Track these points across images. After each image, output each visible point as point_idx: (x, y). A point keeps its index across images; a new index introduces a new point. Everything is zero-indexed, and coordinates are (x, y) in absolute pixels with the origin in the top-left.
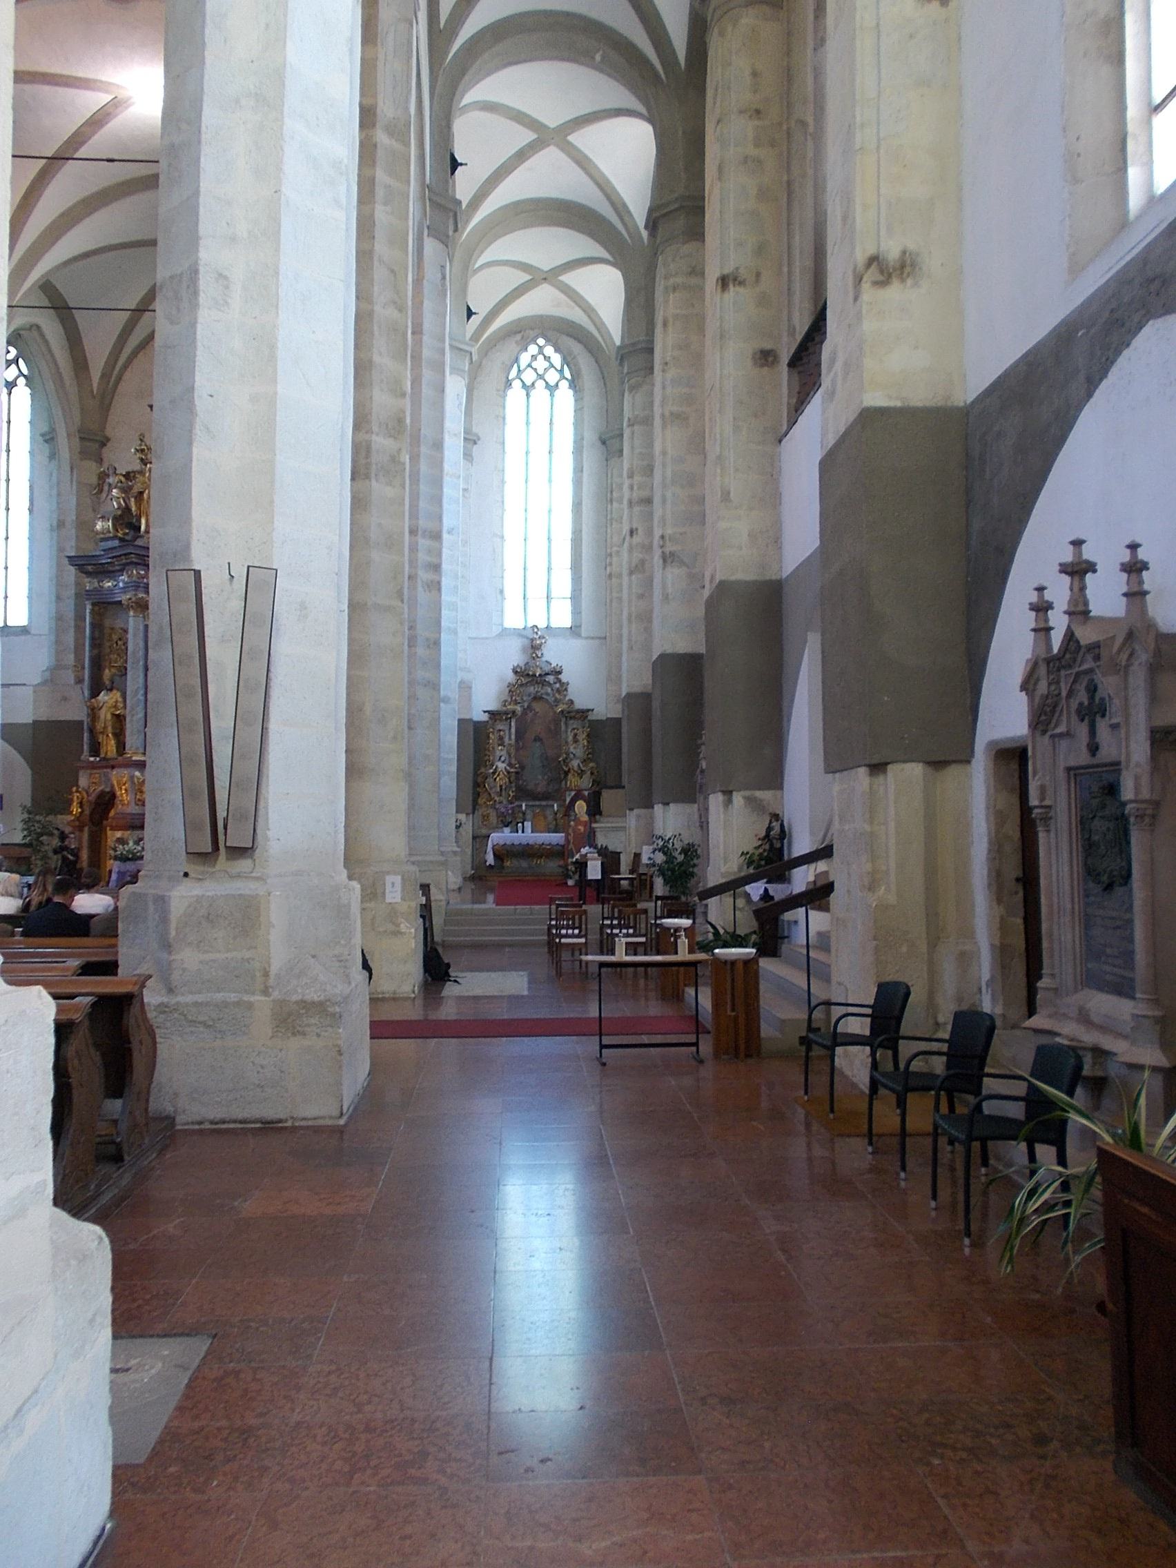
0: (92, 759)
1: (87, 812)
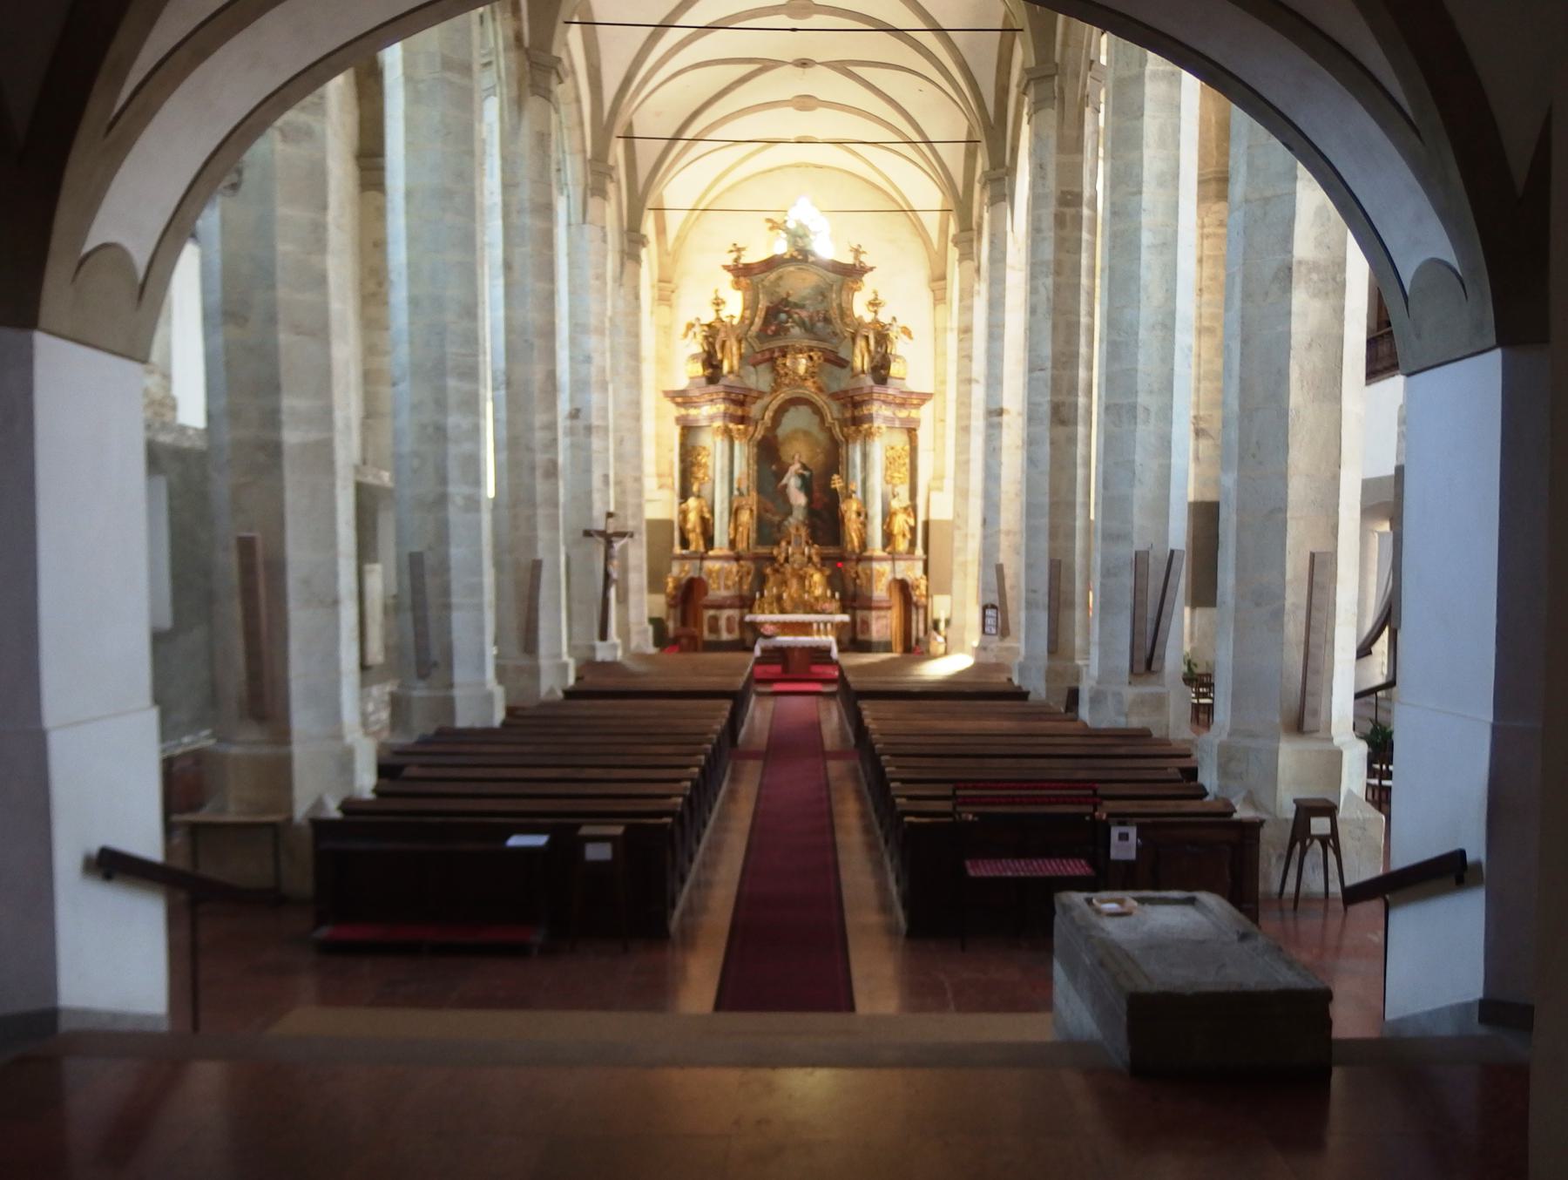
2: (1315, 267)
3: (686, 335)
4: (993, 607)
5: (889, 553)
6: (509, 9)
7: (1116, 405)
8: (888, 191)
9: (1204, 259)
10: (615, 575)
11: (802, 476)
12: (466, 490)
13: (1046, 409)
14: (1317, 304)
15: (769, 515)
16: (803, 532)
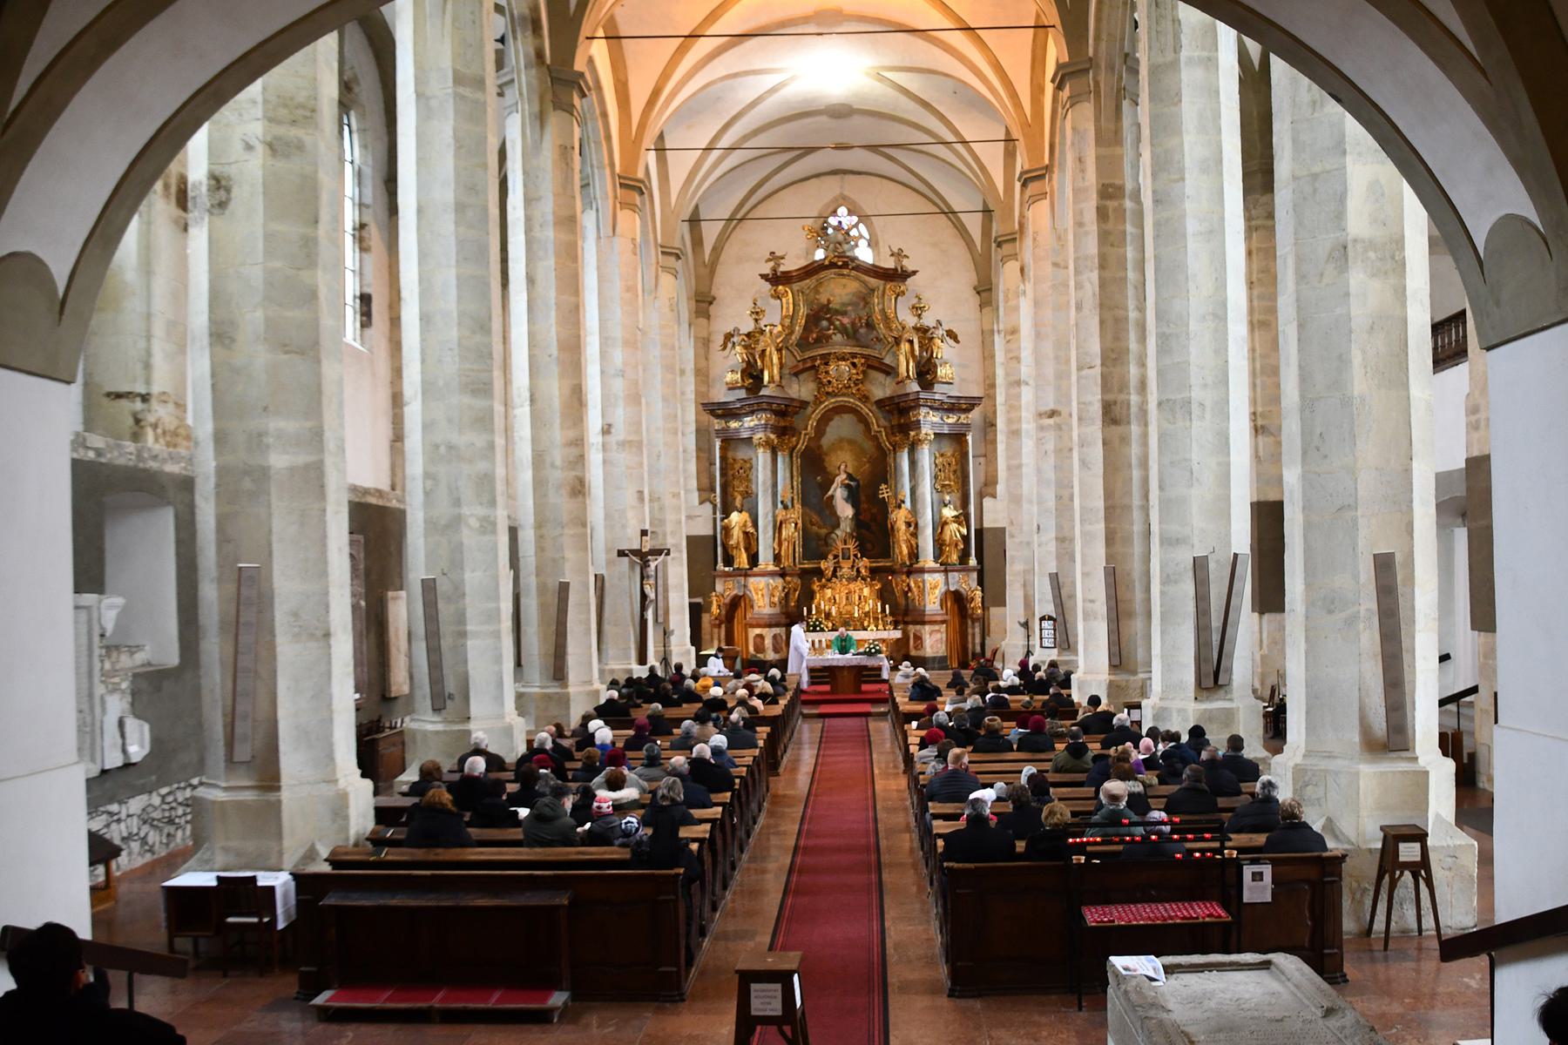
0: (727, 569)
1: (724, 612)
2: (1371, 245)
3: (724, 347)
4: (1050, 618)
6: (530, 27)
7: (1168, 400)
9: (1254, 252)
10: (652, 596)
11: (847, 487)
12: (481, 511)
13: (1096, 409)
14: (1376, 284)
15: (815, 528)
16: (851, 546)
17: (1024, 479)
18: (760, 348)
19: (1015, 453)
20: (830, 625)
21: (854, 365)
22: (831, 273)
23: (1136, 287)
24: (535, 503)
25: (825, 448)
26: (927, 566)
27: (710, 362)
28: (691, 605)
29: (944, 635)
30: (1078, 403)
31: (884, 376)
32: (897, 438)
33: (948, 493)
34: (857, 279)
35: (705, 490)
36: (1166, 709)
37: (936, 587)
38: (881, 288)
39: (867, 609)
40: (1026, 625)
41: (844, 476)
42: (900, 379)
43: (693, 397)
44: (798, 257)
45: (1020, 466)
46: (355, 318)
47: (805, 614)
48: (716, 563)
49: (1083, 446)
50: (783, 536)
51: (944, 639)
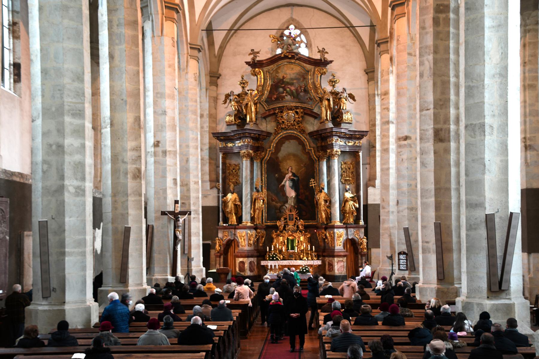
0: (225, 225)
1: (222, 249)
3: (225, 102)
5: (344, 224)
7: (471, 124)
8: (339, 18)
10: (180, 237)
11: (292, 180)
12: (76, 183)
13: (430, 133)
17: (390, 176)
18: (245, 102)
19: (385, 161)
20: (282, 257)
21: (297, 113)
22: (285, 62)
23: (455, 64)
24: (112, 183)
25: (280, 159)
26: (336, 224)
27: (218, 110)
28: (204, 245)
29: (345, 264)
30: (420, 130)
31: (313, 119)
32: (320, 154)
33: (348, 184)
34: (299, 65)
35: (214, 181)
36: (470, 303)
37: (341, 236)
38: (313, 70)
39: (302, 248)
40: (391, 258)
41: (290, 174)
42: (322, 121)
43: (208, 129)
44: (266, 52)
45: (388, 169)
46: (10, 77)
47: (268, 250)
48: (219, 221)
49: (422, 154)
50: (256, 207)
51: (345, 265)
